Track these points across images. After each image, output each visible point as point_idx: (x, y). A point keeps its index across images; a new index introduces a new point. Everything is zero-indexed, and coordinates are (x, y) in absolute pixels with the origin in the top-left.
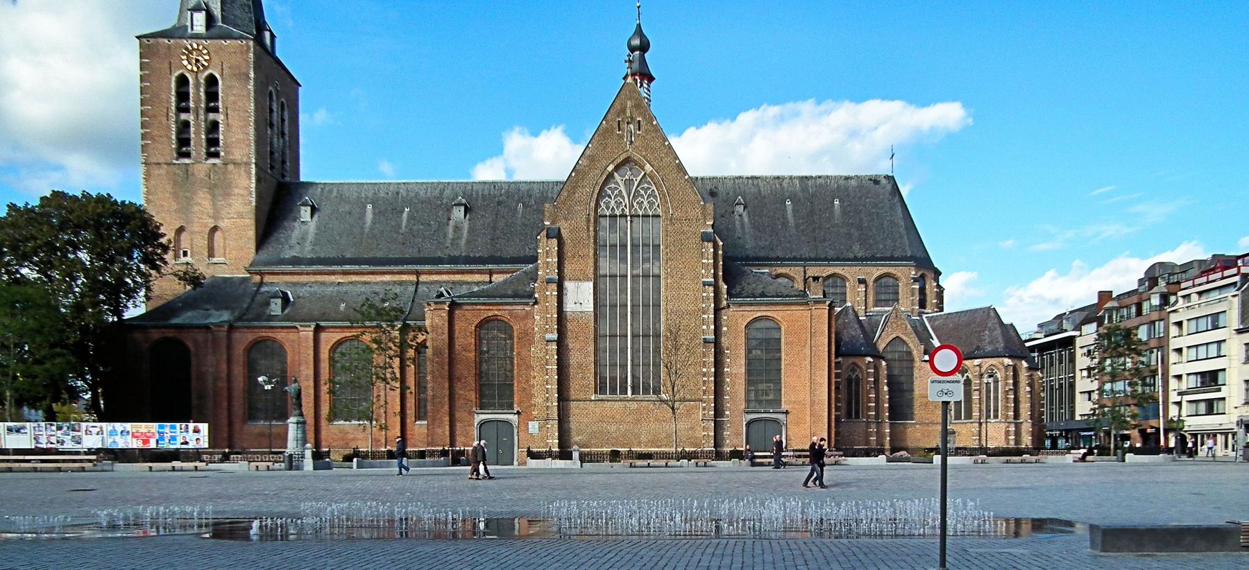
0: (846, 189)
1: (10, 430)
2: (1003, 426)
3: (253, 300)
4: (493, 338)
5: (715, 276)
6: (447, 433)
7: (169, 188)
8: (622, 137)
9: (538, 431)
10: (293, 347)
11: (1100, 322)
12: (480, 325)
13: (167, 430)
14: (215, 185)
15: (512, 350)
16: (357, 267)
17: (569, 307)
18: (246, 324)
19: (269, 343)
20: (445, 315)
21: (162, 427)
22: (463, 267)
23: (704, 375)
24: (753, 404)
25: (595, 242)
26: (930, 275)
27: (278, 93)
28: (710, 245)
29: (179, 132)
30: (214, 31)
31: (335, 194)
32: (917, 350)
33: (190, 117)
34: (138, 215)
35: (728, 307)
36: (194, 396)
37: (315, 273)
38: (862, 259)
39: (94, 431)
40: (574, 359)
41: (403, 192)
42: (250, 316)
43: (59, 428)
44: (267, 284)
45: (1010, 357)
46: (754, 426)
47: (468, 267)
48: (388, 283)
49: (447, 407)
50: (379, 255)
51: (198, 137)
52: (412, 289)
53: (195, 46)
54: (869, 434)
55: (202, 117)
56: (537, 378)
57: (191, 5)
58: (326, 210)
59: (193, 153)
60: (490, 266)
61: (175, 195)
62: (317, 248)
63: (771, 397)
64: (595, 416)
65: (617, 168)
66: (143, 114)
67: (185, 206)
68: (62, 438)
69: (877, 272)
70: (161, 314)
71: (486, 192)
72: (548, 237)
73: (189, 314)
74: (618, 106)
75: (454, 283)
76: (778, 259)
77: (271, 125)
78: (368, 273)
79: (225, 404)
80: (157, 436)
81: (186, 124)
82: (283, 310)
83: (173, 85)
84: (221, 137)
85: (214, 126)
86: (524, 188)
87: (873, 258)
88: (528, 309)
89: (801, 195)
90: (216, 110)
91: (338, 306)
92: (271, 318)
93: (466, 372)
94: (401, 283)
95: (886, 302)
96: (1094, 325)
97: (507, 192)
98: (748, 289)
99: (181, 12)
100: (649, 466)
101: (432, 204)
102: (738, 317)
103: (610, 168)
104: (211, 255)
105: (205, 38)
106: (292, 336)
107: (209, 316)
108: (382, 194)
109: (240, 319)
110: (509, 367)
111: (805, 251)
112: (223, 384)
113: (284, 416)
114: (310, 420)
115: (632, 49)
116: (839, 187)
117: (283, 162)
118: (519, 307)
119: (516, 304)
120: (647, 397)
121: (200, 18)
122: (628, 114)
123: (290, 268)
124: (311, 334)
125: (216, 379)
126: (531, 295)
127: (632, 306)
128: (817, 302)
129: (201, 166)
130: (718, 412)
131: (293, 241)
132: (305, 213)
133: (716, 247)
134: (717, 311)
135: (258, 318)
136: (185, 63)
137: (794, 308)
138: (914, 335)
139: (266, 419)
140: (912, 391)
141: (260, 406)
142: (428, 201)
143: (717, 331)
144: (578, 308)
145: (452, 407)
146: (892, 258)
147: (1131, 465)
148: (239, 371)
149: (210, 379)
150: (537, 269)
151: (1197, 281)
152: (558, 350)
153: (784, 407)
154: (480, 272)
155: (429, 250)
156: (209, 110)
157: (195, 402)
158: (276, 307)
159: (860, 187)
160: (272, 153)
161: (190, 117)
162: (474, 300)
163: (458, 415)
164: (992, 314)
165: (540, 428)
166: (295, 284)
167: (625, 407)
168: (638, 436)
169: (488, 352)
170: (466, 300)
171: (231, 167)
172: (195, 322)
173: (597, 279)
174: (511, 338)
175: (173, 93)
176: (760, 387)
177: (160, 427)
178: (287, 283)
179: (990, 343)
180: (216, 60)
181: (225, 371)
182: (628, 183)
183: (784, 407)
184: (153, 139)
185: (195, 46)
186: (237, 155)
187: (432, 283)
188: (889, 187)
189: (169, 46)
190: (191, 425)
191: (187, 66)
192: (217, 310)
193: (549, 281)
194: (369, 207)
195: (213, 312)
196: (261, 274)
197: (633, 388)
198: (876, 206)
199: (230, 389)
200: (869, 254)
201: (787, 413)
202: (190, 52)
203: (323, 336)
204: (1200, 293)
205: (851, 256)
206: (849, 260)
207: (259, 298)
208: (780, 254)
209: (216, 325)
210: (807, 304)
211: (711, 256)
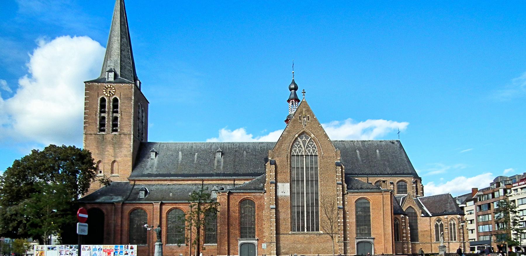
0: (381, 146)
1: (49, 248)
2: (459, 244)
4: (246, 207)
5: (342, 181)
7: (95, 144)
8: (301, 123)
10: (150, 212)
11: (475, 200)
12: (241, 202)
13: (119, 248)
14: (115, 143)
15: (254, 213)
16: (176, 178)
17: (280, 194)
18: (130, 202)
19: (139, 210)
20: (226, 197)
21: (117, 247)
22: (222, 178)
23: (339, 222)
24: (359, 235)
25: (290, 166)
26: (419, 181)
27: (141, 104)
28: (340, 167)
29: (100, 121)
30: (117, 80)
31: (165, 147)
32: (419, 212)
33: (106, 115)
34: (88, 155)
35: (348, 193)
38: (391, 174)
39: (87, 248)
40: (282, 216)
41: (194, 147)
43: (71, 248)
45: (459, 214)
46: (359, 245)
47: (224, 178)
48: (189, 185)
49: (226, 238)
50: (186, 172)
51: (108, 123)
52: (201, 187)
53: (109, 86)
54: (404, 248)
55: (111, 115)
56: (266, 225)
57: (107, 70)
58: (161, 154)
59: (106, 130)
60: (234, 177)
61: (98, 147)
62: (159, 170)
65: (299, 136)
66: (85, 113)
67: (102, 152)
68: (72, 252)
69: (398, 179)
71: (230, 147)
72: (271, 164)
73: (104, 198)
74: (299, 110)
75: (218, 184)
76: (356, 174)
77: (139, 118)
78: (181, 180)
79: (119, 237)
80: (114, 251)
81: (104, 118)
82: (145, 196)
83: (99, 102)
84: (119, 123)
85: (116, 119)
86: (246, 145)
87: (396, 174)
88: (262, 195)
89: (362, 148)
90: (117, 112)
91: (169, 195)
92: (140, 199)
93: (235, 223)
94: (196, 184)
95: (402, 192)
96: (473, 202)
97: (239, 147)
98: (355, 186)
99: (102, 72)
101: (209, 152)
102: (352, 198)
103: (297, 136)
104: (112, 173)
105: (114, 83)
106: (151, 207)
107: (112, 199)
108: (185, 147)
109: (126, 200)
110: (253, 219)
111: (367, 171)
112: (119, 228)
115: (291, 89)
116: (378, 145)
117: (142, 134)
119: (256, 193)
120: (313, 232)
121: (112, 75)
122: (304, 114)
123: (147, 178)
126: (262, 189)
127: (306, 193)
128: (385, 191)
129: (109, 135)
130: (345, 239)
131: (148, 167)
132: (153, 155)
133: (342, 168)
134: (343, 195)
135: (135, 199)
136: (105, 93)
138: (417, 206)
141: (134, 238)
142: (205, 150)
144: (283, 194)
145: (228, 237)
146: (403, 174)
149: (113, 225)
150: (265, 178)
151: (520, 183)
153: (372, 236)
154: (230, 180)
155: (207, 170)
156: (114, 112)
157: (105, 236)
158: (142, 195)
159: (387, 145)
160: (139, 130)
161: (106, 115)
162: (238, 191)
163: (231, 241)
165: (267, 246)
166: (149, 185)
167: (304, 237)
168: (309, 249)
169: (244, 213)
171: (122, 136)
173: (292, 182)
174: (254, 208)
175: (99, 105)
176: (361, 227)
178: (145, 184)
179: (451, 208)
180: (118, 92)
181: (120, 222)
182: (304, 142)
183: (372, 236)
184: (89, 124)
185: (109, 86)
186: (125, 131)
188: (398, 145)
189: (98, 86)
190: (130, 246)
191: (105, 94)
192: (116, 196)
193: (272, 183)
194: (180, 153)
196: (135, 181)
198: (394, 153)
199: (122, 231)
200: (393, 172)
201: (374, 239)
202: (107, 89)
204: (522, 188)
205: (386, 173)
206: (379, 174)
207: (133, 191)
208: (357, 172)
209: (117, 202)
210: (381, 192)
211: (340, 172)
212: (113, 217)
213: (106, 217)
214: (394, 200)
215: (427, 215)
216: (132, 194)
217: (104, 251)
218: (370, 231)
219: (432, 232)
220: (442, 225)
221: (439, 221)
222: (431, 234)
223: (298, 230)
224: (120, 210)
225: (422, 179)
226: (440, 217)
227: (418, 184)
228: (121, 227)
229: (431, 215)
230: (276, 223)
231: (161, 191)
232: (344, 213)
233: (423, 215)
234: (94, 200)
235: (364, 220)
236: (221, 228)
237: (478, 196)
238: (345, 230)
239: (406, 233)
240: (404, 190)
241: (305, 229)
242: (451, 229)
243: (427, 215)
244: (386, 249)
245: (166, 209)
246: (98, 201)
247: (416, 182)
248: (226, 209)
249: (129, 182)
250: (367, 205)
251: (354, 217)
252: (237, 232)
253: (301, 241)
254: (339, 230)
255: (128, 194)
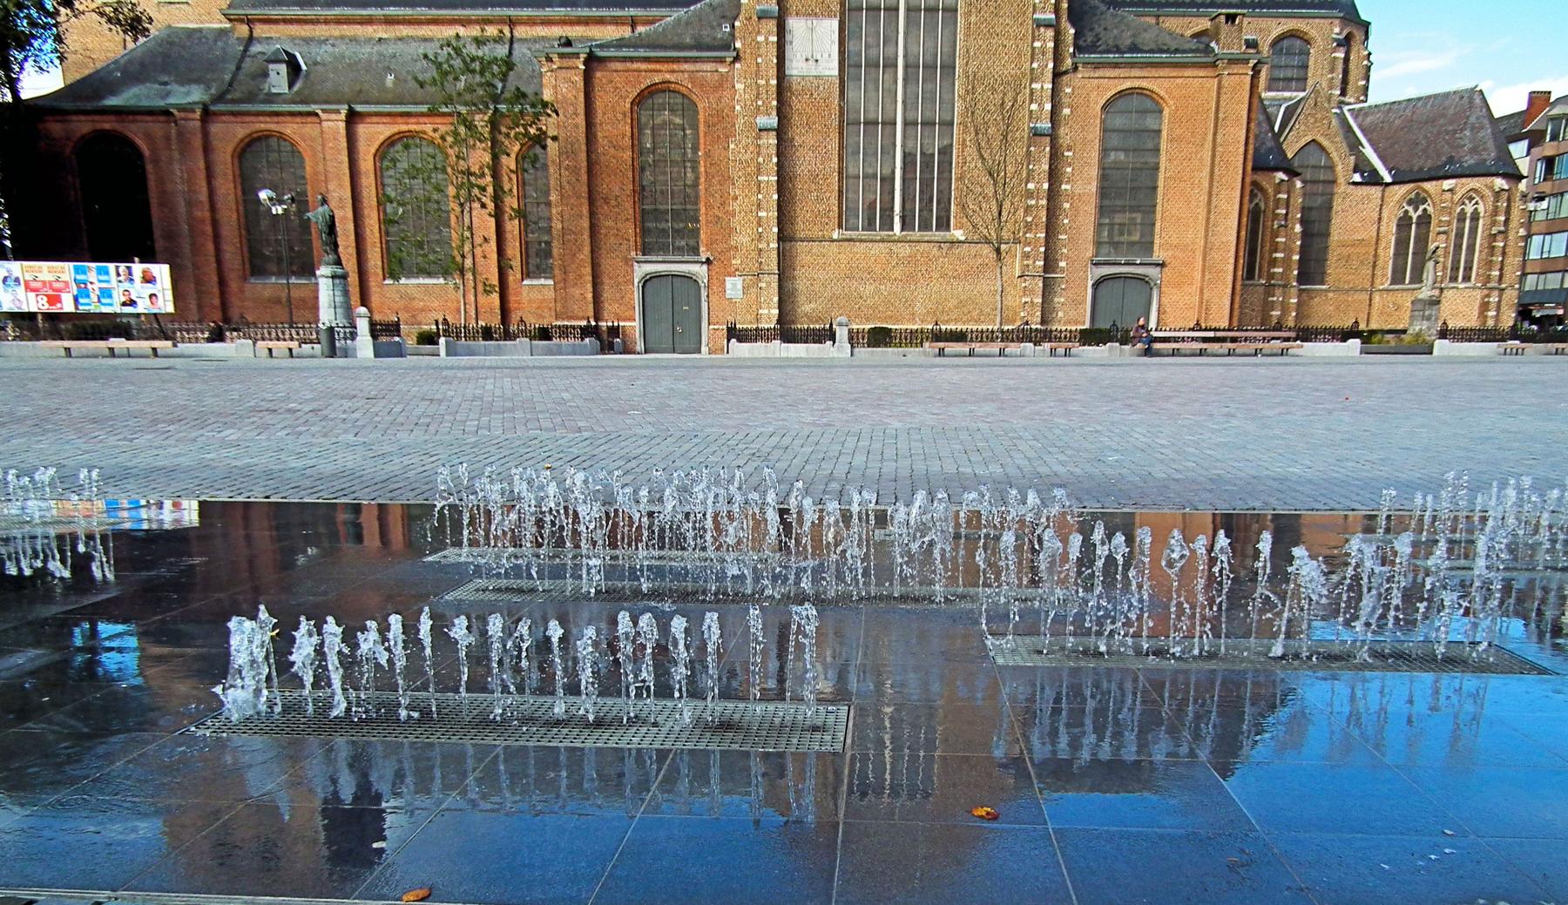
2: (1478, 294)
3: (239, 68)
6: (590, 296)
9: (743, 294)
10: (313, 149)
15: (695, 149)
19: (273, 142)
20: (579, 80)
23: (1030, 194)
24: (1105, 249)
26: (1359, 36)
35: (1075, 69)
36: (157, 233)
37: (339, 21)
42: (237, 95)
44: (259, 40)
46: (1103, 289)
49: (587, 250)
60: (632, 12)
63: (1136, 237)
64: (843, 271)
70: (84, 93)
79: (210, 247)
82: (291, 86)
88: (723, 69)
91: (383, 80)
92: (271, 98)
93: (618, 186)
100: (971, 354)
102: (1093, 89)
107: (168, 94)
109: (220, 98)
113: (308, 269)
114: (350, 264)
118: (708, 67)
120: (927, 235)
124: (342, 125)
125: (190, 204)
126: (727, 45)
128: (1233, 61)
130: (1050, 264)
134: (1057, 75)
135: (251, 98)
137: (1188, 72)
139: (279, 274)
140: (1328, 235)
143: (1054, 114)
144: (811, 70)
147: (1450, 361)
148: (227, 189)
149: (182, 208)
152: (778, 145)
153: (1158, 255)
154: (616, 21)
158: (278, 79)
162: (625, 53)
164: (1478, 100)
166: (307, 41)
168: (909, 304)
170: (612, 53)
172: (145, 103)
174: (695, 127)
176: (1119, 218)
177: (77, 270)
178: (293, 39)
183: (1158, 255)
187: (535, 40)
190: (138, 268)
192: (182, 84)
193: (763, 16)
195: (175, 87)
196: (250, 22)
197: (903, 219)
199: (215, 223)
201: (1162, 265)
203: (362, 130)
207: (248, 65)
209: (182, 108)
210: (1214, 65)
212: (177, 167)
213: (149, 167)
214: (1257, 109)
215: (1373, 179)
216: (241, 77)
217: (28, 288)
218: (1152, 234)
219: (1382, 245)
220: (1425, 220)
221: (1416, 202)
222: (1376, 256)
223: (870, 225)
224: (197, 142)
225: (1373, 30)
226: (1427, 186)
227: (1354, 49)
228: (213, 208)
229: (1388, 179)
230: (779, 192)
231: (353, 65)
232: (1055, 156)
233: (1357, 178)
234: (102, 98)
235: (1129, 195)
236: (564, 213)
237: (1553, 119)
238: (1051, 228)
239: (1288, 250)
240: (1294, 73)
241: (897, 220)
242: (1460, 235)
243: (1373, 179)
244: (1205, 307)
245: (370, 140)
246: (112, 101)
247: (1346, 42)
248: (582, 128)
249: (232, 30)
250: (1150, 122)
251: (1094, 172)
252: (630, 230)
253: (878, 270)
254: (1028, 227)
255: (227, 77)
